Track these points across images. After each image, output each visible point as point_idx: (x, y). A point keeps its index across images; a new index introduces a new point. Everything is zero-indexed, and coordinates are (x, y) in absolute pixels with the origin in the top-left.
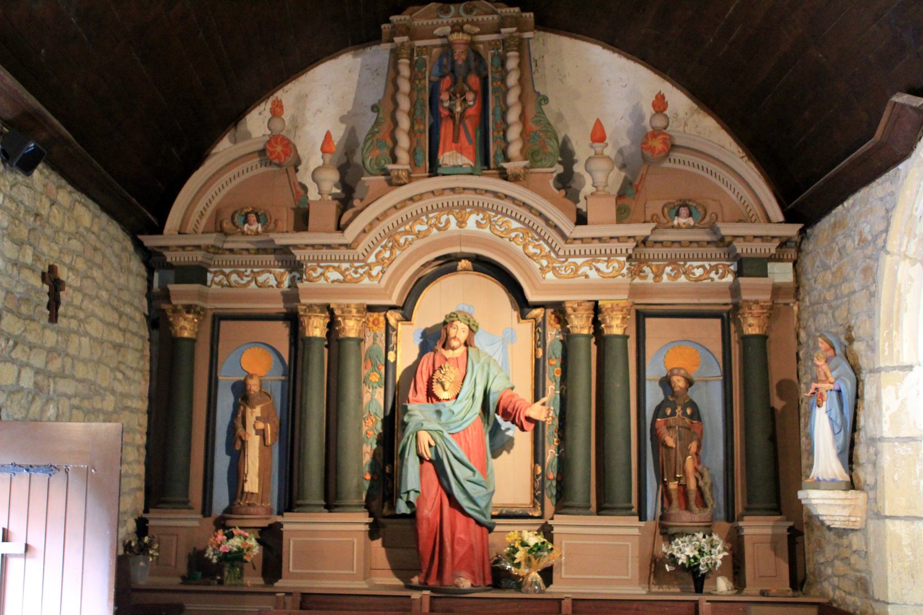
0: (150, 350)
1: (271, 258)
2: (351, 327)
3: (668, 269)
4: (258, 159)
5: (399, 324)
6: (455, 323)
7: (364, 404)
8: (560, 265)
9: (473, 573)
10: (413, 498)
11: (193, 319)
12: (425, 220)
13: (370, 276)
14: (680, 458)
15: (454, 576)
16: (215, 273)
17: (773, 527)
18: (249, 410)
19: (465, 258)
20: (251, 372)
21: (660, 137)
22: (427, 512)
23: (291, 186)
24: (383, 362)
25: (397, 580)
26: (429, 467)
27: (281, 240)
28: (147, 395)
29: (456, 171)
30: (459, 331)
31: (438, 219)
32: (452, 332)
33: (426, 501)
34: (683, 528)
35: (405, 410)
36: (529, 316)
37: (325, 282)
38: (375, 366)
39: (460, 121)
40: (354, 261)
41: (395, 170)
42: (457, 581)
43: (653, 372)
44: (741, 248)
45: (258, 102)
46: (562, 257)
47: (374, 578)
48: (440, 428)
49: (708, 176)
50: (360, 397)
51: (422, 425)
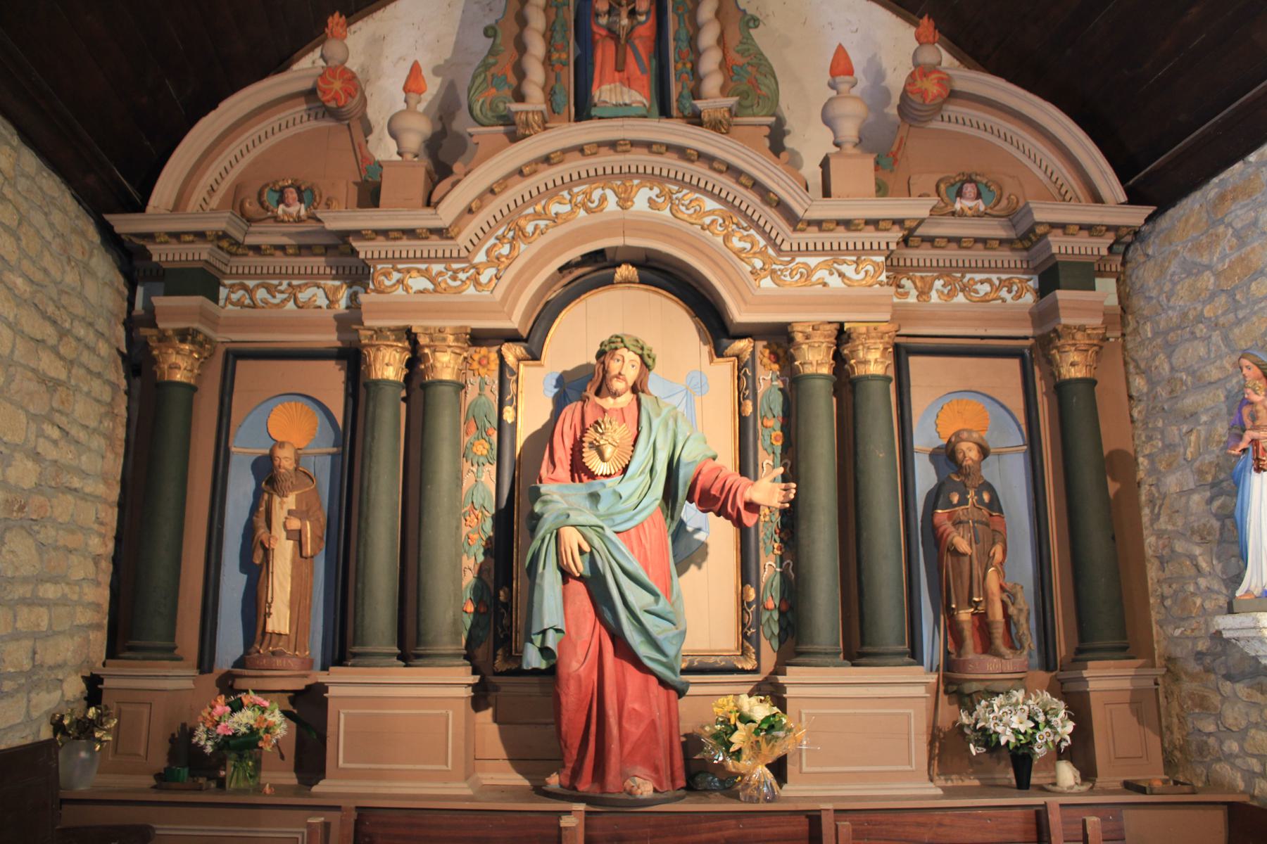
0: (128, 409)
1: (318, 262)
2: (445, 365)
3: (938, 284)
4: (305, 107)
5: (521, 366)
6: (618, 352)
7: (464, 491)
8: (782, 267)
9: (656, 769)
10: (552, 641)
11: (191, 352)
12: (568, 197)
13: (477, 283)
14: (977, 571)
15: (624, 776)
16: (232, 286)
17: (1134, 677)
18: (277, 499)
19: (626, 262)
20: (280, 439)
21: (935, 76)
22: (577, 665)
23: (354, 150)
24: (495, 424)
25: (519, 776)
26: (578, 588)
27: (340, 219)
28: (119, 478)
29: (622, 112)
30: (626, 366)
31: (588, 195)
32: (614, 367)
33: (575, 646)
34: (988, 683)
35: (536, 495)
36: (729, 351)
37: (404, 293)
38: (482, 432)
39: (627, 42)
40: (452, 259)
41: (522, 112)
42: (629, 783)
43: (925, 438)
44: (1059, 245)
45: (310, 45)
46: (786, 253)
47: (480, 775)
48: (595, 521)
49: (999, 142)
50: (458, 479)
51: (568, 516)
